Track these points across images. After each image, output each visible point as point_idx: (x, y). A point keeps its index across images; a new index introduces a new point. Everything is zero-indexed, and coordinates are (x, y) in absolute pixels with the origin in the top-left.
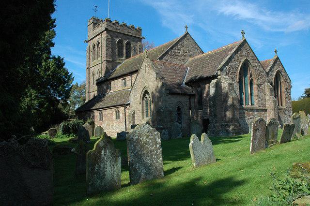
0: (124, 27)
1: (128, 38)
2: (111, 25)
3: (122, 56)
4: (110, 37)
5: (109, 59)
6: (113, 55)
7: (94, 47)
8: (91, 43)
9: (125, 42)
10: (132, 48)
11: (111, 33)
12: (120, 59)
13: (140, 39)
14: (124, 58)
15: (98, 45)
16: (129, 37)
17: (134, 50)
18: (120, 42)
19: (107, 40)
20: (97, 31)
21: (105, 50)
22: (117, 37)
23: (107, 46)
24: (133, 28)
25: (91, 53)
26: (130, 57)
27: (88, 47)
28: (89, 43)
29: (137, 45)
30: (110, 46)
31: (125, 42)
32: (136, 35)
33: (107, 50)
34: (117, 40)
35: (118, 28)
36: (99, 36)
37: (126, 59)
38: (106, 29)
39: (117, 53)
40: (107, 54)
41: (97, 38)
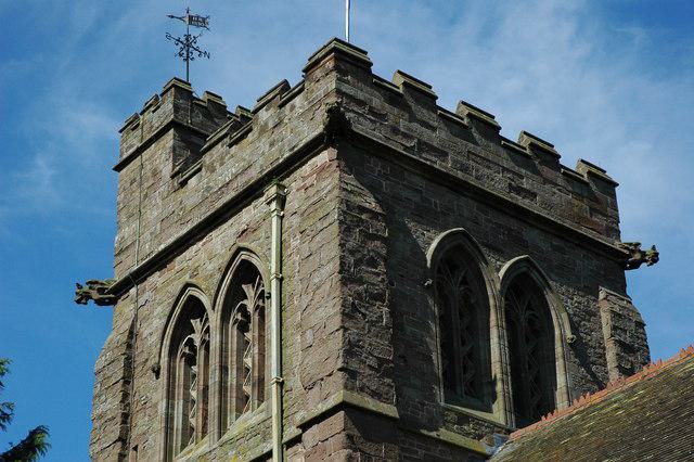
0: (484, 147)
1: (520, 244)
2: (377, 102)
3: (480, 393)
4: (371, 203)
5: (371, 404)
6: (401, 369)
7: (182, 328)
8: (154, 304)
9: (497, 272)
10: (562, 330)
11: (376, 166)
12: (463, 419)
13: (616, 263)
14: (498, 414)
15: (235, 296)
16: (531, 235)
17: (578, 348)
18: (459, 261)
19: (351, 219)
20: (226, 172)
21: (329, 311)
22: (433, 220)
23: (347, 276)
24: (488, 128)
25: (150, 390)
26: (547, 406)
27: (117, 335)
28: (125, 307)
29: (593, 314)
30: (376, 277)
31: (497, 272)
32: (580, 220)
33: (349, 313)
34: (432, 244)
35: (427, 135)
36: (247, 215)
37: (520, 425)
38: (337, 133)
39: (436, 358)
40: (351, 350)
41: (221, 241)
